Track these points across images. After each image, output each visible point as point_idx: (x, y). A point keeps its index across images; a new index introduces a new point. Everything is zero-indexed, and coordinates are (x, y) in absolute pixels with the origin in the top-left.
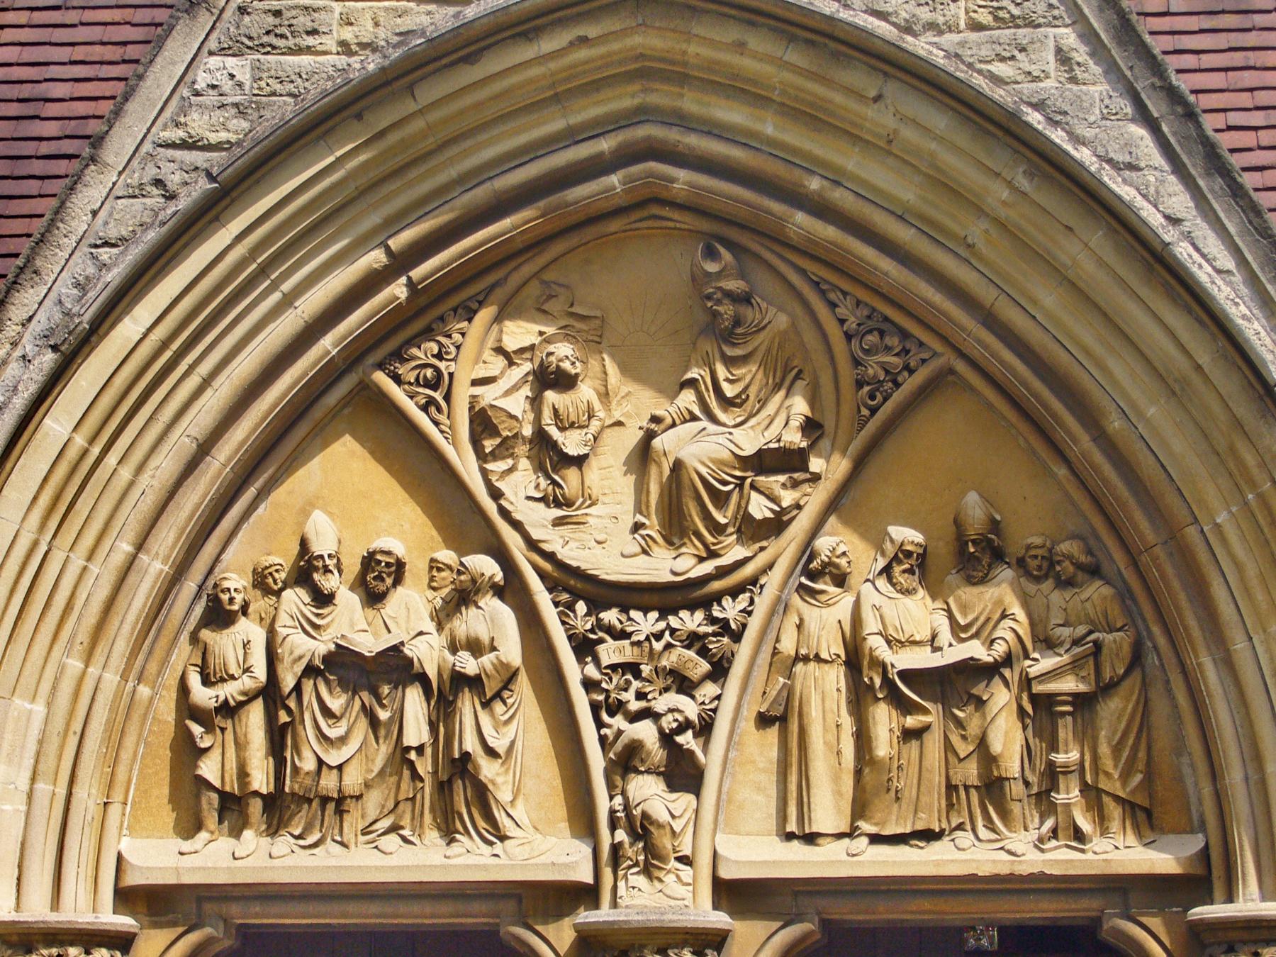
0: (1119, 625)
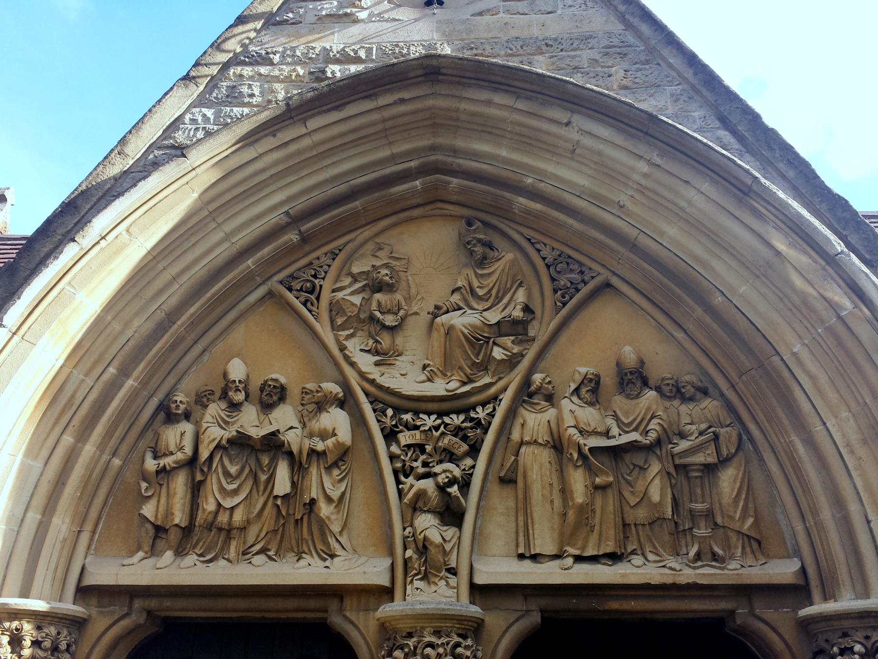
0: (728, 423)
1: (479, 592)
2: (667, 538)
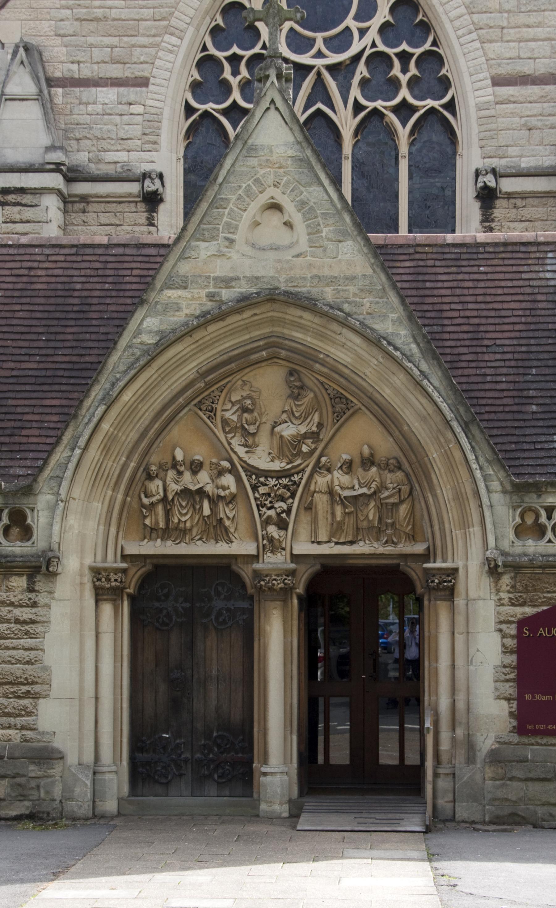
1: (295, 558)
2: (374, 534)
